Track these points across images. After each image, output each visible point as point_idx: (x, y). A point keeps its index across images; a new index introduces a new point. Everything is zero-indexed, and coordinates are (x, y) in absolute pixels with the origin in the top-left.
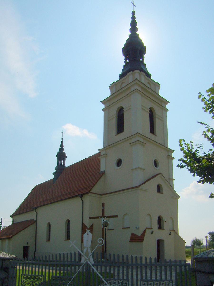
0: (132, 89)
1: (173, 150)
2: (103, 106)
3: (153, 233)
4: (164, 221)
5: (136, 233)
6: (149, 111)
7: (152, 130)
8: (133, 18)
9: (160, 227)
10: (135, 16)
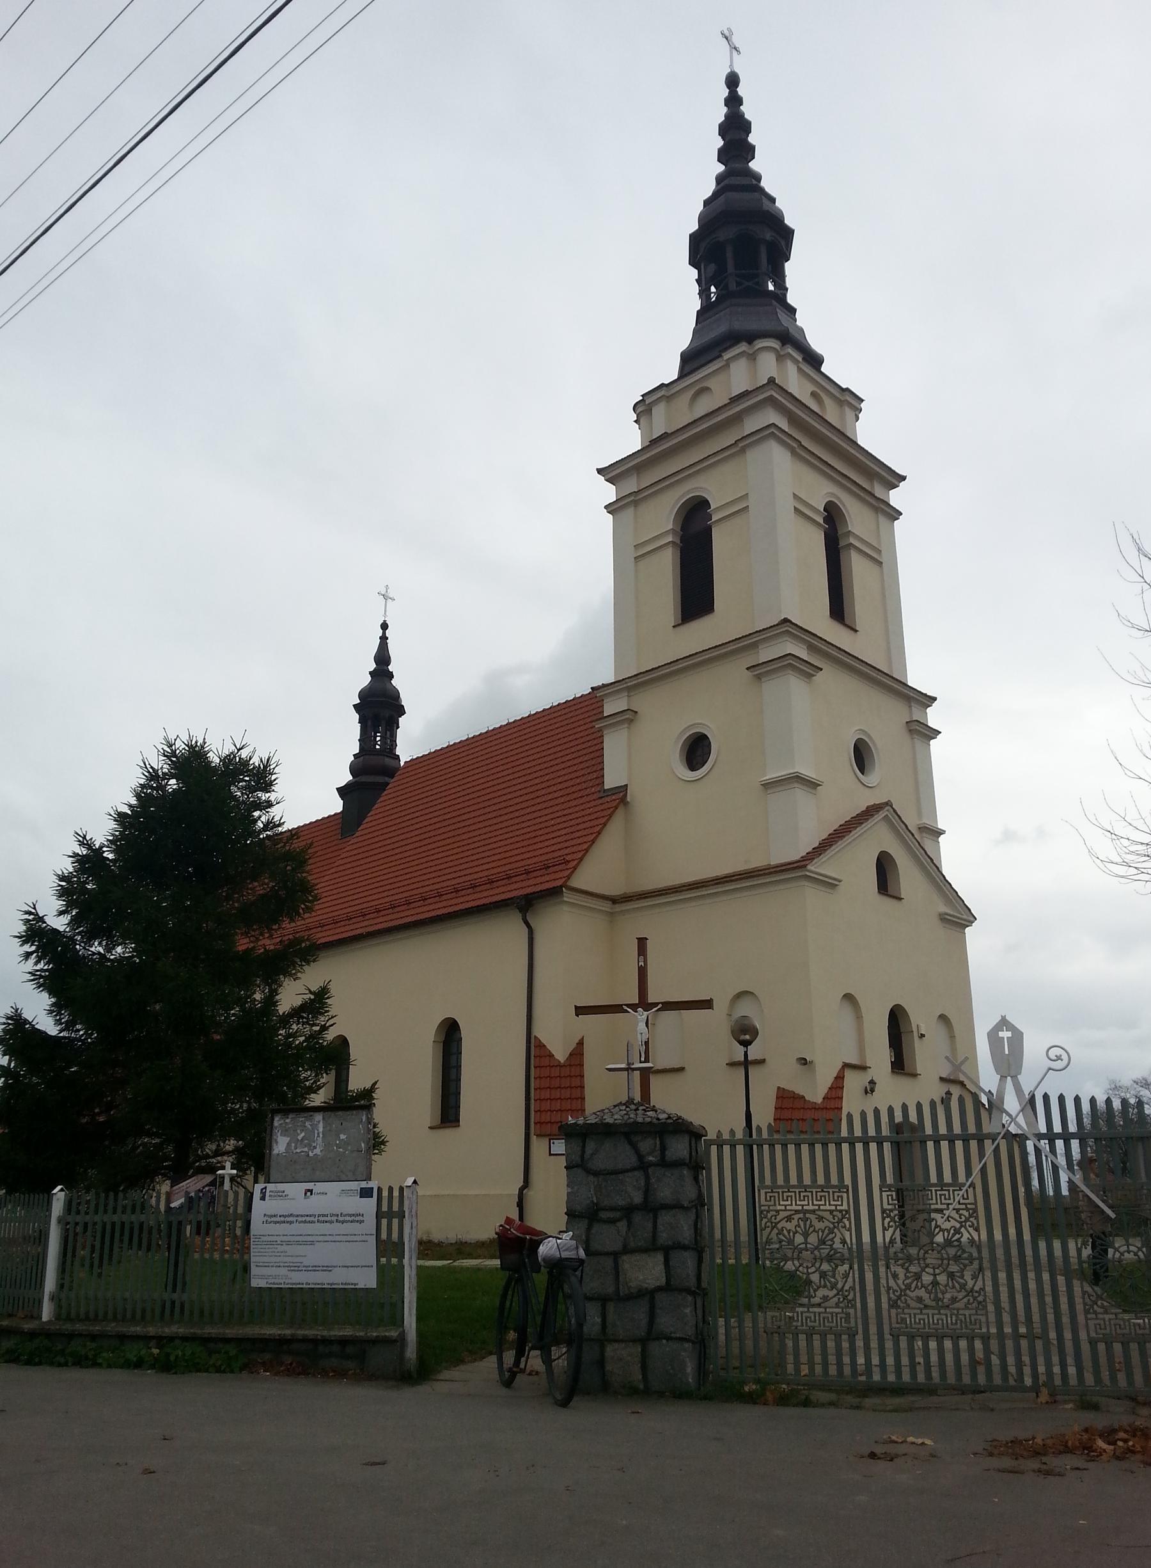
0: (752, 424)
1: (930, 697)
3: (872, 1091)
4: (915, 1034)
5: (800, 1090)
7: (839, 609)
8: (734, 101)
9: (900, 1065)
10: (741, 90)
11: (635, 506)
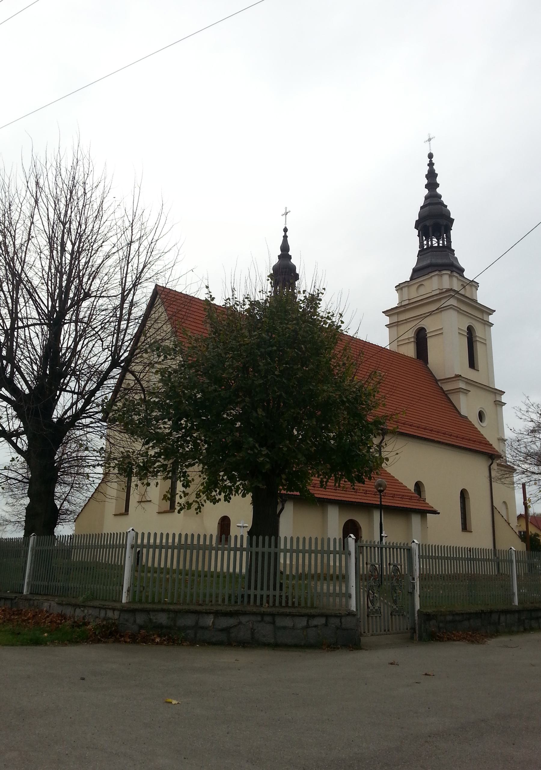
1: (501, 391)
2: (387, 320)
6: (466, 334)
7: (472, 364)
11: (398, 314)
